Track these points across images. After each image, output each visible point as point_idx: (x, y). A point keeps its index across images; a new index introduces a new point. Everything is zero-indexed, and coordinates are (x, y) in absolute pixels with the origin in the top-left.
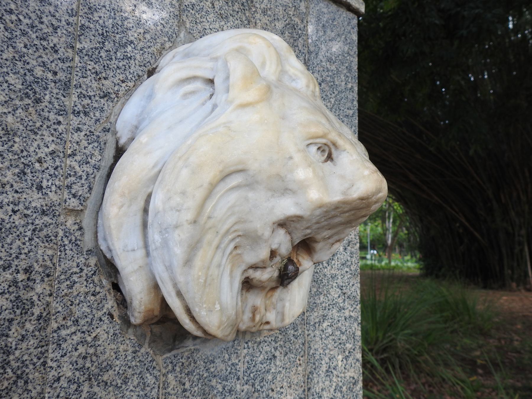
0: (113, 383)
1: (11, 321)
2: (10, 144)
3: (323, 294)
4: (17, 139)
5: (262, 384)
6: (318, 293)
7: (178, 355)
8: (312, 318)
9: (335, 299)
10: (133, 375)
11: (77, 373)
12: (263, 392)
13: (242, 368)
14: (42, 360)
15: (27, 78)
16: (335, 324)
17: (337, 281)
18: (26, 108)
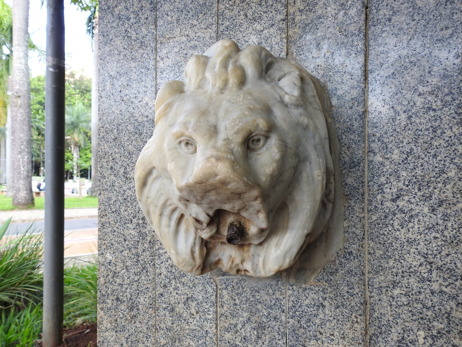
0: (188, 285)
1: (138, 242)
2: (131, 159)
3: (393, 259)
4: (134, 156)
5: (309, 324)
6: (386, 256)
7: (229, 279)
8: (376, 280)
9: (413, 266)
10: (199, 283)
11: (169, 273)
12: (310, 331)
13: (287, 305)
14: (153, 263)
15: (135, 124)
16: (412, 294)
17: (418, 247)
18: (136, 140)
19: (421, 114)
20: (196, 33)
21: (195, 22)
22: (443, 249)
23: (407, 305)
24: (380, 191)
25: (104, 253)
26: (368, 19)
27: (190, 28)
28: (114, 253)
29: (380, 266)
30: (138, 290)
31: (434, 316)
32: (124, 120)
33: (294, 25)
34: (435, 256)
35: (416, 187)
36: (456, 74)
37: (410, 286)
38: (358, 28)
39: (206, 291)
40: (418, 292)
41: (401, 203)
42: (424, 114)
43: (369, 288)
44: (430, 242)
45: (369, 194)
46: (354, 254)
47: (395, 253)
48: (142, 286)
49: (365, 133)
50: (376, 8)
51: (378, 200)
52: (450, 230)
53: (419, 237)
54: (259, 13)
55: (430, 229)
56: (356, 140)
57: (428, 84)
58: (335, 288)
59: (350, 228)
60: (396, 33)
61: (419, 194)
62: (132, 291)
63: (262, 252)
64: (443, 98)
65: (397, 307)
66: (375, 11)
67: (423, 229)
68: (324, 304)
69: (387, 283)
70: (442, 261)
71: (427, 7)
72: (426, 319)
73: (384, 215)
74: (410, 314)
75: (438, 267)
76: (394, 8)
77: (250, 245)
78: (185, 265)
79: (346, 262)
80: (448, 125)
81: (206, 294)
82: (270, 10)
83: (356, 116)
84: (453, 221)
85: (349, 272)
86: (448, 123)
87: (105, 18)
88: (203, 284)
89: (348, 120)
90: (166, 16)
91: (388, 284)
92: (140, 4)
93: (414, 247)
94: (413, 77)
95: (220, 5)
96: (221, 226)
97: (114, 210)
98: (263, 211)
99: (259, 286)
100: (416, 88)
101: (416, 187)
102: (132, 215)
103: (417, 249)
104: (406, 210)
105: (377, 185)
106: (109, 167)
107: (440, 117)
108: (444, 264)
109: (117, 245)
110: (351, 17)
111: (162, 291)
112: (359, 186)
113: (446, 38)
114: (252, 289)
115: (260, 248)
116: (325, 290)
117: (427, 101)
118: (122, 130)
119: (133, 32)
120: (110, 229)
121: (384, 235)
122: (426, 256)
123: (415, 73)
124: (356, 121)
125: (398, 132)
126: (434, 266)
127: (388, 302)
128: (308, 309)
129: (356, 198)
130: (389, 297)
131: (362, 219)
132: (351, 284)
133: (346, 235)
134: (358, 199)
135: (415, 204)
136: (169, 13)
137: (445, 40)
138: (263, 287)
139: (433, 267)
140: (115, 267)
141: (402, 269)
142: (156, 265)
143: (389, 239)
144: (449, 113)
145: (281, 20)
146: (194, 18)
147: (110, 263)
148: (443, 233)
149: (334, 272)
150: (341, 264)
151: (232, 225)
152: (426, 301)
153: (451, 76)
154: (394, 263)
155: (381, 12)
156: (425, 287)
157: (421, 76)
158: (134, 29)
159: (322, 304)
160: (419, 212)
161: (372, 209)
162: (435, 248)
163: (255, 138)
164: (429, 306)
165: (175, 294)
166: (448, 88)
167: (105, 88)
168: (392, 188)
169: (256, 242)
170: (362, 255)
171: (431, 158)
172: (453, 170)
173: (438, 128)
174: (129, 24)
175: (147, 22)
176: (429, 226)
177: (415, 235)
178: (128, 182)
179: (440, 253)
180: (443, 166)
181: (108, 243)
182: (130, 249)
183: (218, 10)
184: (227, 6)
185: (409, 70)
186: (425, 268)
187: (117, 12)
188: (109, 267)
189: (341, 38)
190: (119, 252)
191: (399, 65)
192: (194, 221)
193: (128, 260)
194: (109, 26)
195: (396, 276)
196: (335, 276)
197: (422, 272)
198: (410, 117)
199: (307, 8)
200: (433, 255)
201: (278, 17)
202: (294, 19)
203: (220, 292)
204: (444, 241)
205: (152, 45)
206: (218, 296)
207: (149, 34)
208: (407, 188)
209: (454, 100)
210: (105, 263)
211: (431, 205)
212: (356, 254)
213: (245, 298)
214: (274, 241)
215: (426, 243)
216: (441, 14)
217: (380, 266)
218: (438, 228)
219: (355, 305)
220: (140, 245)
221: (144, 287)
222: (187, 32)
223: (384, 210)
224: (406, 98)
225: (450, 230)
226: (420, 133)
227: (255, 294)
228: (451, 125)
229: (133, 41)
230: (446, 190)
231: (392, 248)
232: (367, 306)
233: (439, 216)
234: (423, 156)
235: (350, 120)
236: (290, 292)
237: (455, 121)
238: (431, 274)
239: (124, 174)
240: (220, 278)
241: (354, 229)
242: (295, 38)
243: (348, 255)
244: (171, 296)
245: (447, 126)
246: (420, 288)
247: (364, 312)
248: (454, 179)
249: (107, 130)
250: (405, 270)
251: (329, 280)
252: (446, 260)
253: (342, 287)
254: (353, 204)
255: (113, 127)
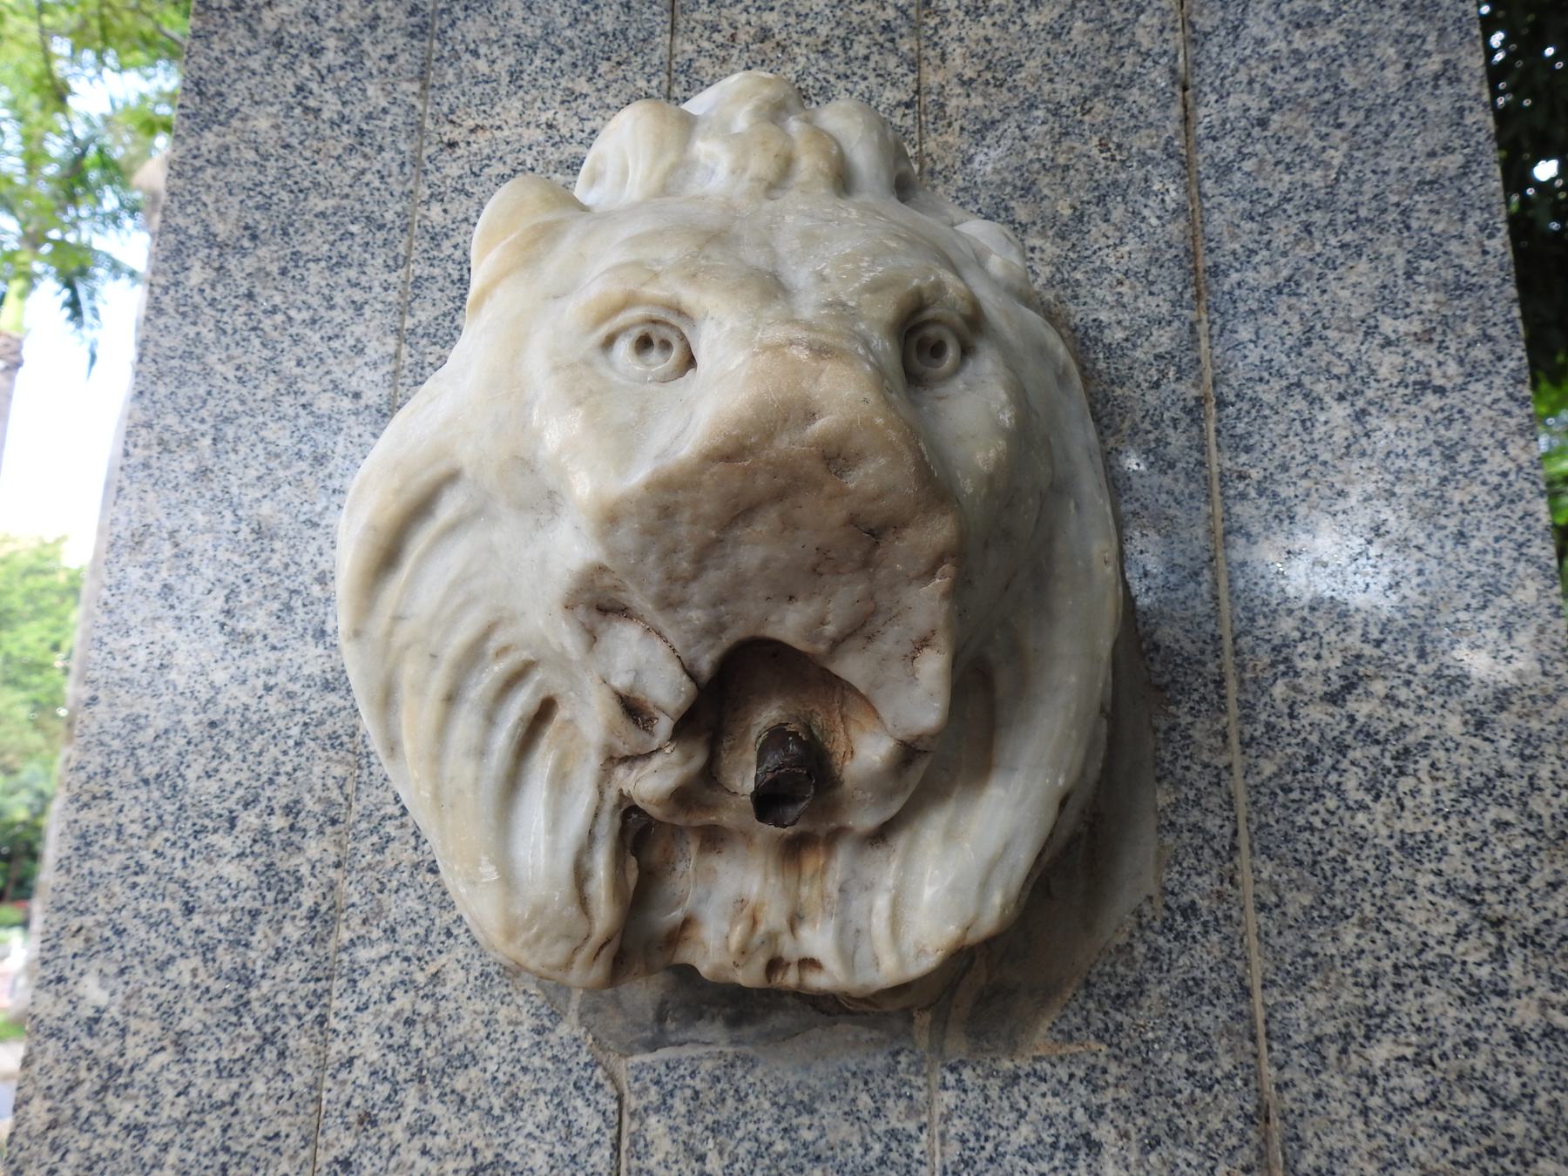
0: (483, 1103)
1: (254, 914)
2: (264, 556)
3: (1354, 920)
6: (1326, 912)
7: (679, 1062)
9: (1432, 942)
10: (535, 1092)
11: (392, 1057)
13: (938, 1159)
14: (316, 1011)
16: (1443, 1056)
17: (1443, 866)
19: (1397, 402)
20: (582, 120)
21: (582, 86)
22: (1535, 864)
23: (1427, 1102)
24: (1282, 667)
25: (67, 973)
26: (1192, 120)
27: (563, 102)
28: (122, 972)
29: (1307, 953)
30: (227, 1150)
31: (1536, 1134)
32: (251, 403)
33: (945, 122)
34: (1509, 893)
35: (1410, 646)
36: (1494, 281)
37: (1431, 1023)
38: (1162, 142)
39: (569, 1125)
40: (1466, 1043)
41: (1362, 708)
42: (1408, 403)
43: (1270, 1049)
44: (1485, 844)
45: (1242, 682)
46: (1204, 912)
47: (1359, 895)
48: (251, 1129)
49: (1209, 469)
50: (1214, 90)
51: (1278, 702)
52: (1548, 794)
53: (1441, 828)
54: (820, 76)
55: (1474, 793)
56: (1182, 493)
57: (1408, 311)
58: (1138, 1060)
59: (1182, 811)
60: (1288, 160)
61: (1421, 669)
62: (191, 1157)
63: (886, 870)
64: (1462, 353)
65: (1390, 1116)
66: (1213, 97)
67: (1453, 796)
68: (1095, 1135)
69: (1341, 1021)
70: (1536, 911)
71: (1379, 90)
72: (1507, 1153)
73: (1304, 753)
74: (1444, 1141)
75: (1525, 936)
76: (1271, 90)
77: (834, 837)
78: (538, 938)
79: (1176, 946)
80: (1492, 435)
81: (566, 1140)
82: (860, 72)
83: (1176, 412)
84: (1553, 759)
85: (1190, 987)
86: (1490, 429)
87: (215, 38)
88: (556, 1092)
89: (1146, 425)
90: (467, 56)
91: (1347, 1025)
92: (369, 10)
93: (1428, 866)
94: (1359, 290)
95: (678, 41)
96: (726, 745)
97: (150, 771)
98: (941, 640)
99: (812, 1082)
100: (1372, 322)
101: (1410, 646)
102: (240, 792)
103: (1439, 873)
104: (1383, 732)
105: (1267, 647)
106: (156, 586)
107: (1461, 411)
108: (1547, 922)
109: (142, 934)
110: (1135, 111)
111: (349, 1143)
112: (1202, 652)
113: (1450, 179)
114: (782, 1100)
115: (879, 853)
116: (1098, 1073)
117: (1412, 364)
118: (238, 439)
119: (328, 96)
120: (119, 859)
121: (1311, 828)
122: (1477, 898)
123: (1363, 279)
124: (1175, 428)
125: (1325, 463)
126: (1509, 933)
127: (1352, 1099)
128: (1030, 1168)
129: (1196, 696)
130: (1354, 1079)
131: (1225, 775)
132: (1200, 1039)
133: (1169, 839)
134: (1203, 698)
135: (1413, 706)
136: (483, 50)
137: (1447, 183)
138: (830, 1087)
139: (1509, 937)
140: (117, 1044)
141: (1393, 956)
142: (334, 1022)
143: (1331, 844)
144: (1488, 400)
145: (899, 104)
146: (578, 71)
147: (97, 1020)
148: (1525, 804)
149: (1130, 994)
150: (1155, 955)
151: (777, 736)
152: (1501, 1079)
153: (1481, 287)
154: (1359, 936)
155: (1233, 101)
156: (1489, 1019)
157: (1385, 287)
158: (333, 85)
159: (1086, 1137)
160: (1431, 733)
161: (1257, 734)
162: (1506, 865)
163: (931, 332)
164: (1511, 1098)
165: (415, 1156)
166: (1474, 323)
167: (181, 277)
168: (1325, 653)
169: (865, 819)
170: (1235, 913)
171: (1449, 544)
172: (1528, 583)
173: (1459, 447)
174: (313, 67)
175: (392, 68)
176: (1474, 784)
177: (1424, 820)
178: (236, 653)
179: (1525, 880)
180: (1491, 571)
181: (99, 924)
182: (207, 951)
183: (672, 56)
184: (706, 45)
185: (1341, 270)
186: (1478, 943)
187: (272, 25)
188: (87, 1043)
189: (1106, 167)
190: (150, 967)
191: (1304, 253)
192: (615, 710)
193: (190, 1003)
194: (231, 64)
195: (1374, 986)
196: (1133, 1011)
197: (1470, 959)
198: (1359, 417)
199: (988, 75)
200: (1503, 892)
201: (887, 94)
202: (942, 106)
203: (635, 1126)
204: (1532, 834)
205: (403, 147)
206: (625, 1144)
207: (394, 109)
208: (1377, 653)
209: (1500, 359)
210: (70, 1022)
211: (1468, 707)
212: (1211, 912)
213: (747, 1145)
214: (932, 830)
215: (1472, 846)
216: (1424, 110)
217: (1307, 953)
218: (1507, 787)
219: (1220, 1126)
220: (261, 929)
221: (259, 1135)
222: (550, 114)
223: (1303, 735)
224: (1340, 355)
225: (1548, 794)
226: (1400, 463)
227: (795, 1122)
228: (1500, 435)
229: (327, 126)
230: (1515, 653)
231: (1348, 878)
232: (1271, 1127)
233: (1504, 744)
234: (1421, 539)
235: (1156, 425)
236: (949, 1098)
237: (1513, 422)
238: (1504, 967)
239: (221, 618)
240: (636, 1059)
241: (1195, 815)
242: (949, 161)
243: (1179, 919)
244: (392, 1164)
245: (1487, 441)
246: (1468, 1026)
247: (1262, 1154)
248: (1537, 610)
249: (167, 436)
250: (1403, 959)
251: (1112, 1027)
252: (1551, 905)
253: (1166, 1056)
254: (1185, 720)
255: (196, 425)
